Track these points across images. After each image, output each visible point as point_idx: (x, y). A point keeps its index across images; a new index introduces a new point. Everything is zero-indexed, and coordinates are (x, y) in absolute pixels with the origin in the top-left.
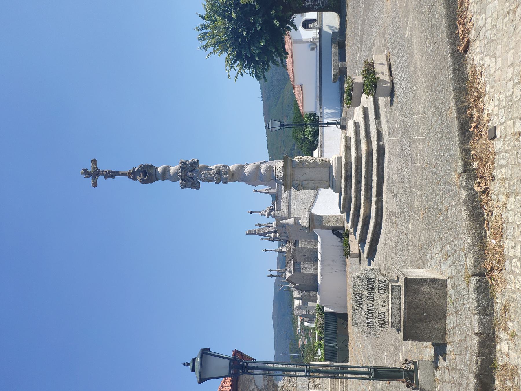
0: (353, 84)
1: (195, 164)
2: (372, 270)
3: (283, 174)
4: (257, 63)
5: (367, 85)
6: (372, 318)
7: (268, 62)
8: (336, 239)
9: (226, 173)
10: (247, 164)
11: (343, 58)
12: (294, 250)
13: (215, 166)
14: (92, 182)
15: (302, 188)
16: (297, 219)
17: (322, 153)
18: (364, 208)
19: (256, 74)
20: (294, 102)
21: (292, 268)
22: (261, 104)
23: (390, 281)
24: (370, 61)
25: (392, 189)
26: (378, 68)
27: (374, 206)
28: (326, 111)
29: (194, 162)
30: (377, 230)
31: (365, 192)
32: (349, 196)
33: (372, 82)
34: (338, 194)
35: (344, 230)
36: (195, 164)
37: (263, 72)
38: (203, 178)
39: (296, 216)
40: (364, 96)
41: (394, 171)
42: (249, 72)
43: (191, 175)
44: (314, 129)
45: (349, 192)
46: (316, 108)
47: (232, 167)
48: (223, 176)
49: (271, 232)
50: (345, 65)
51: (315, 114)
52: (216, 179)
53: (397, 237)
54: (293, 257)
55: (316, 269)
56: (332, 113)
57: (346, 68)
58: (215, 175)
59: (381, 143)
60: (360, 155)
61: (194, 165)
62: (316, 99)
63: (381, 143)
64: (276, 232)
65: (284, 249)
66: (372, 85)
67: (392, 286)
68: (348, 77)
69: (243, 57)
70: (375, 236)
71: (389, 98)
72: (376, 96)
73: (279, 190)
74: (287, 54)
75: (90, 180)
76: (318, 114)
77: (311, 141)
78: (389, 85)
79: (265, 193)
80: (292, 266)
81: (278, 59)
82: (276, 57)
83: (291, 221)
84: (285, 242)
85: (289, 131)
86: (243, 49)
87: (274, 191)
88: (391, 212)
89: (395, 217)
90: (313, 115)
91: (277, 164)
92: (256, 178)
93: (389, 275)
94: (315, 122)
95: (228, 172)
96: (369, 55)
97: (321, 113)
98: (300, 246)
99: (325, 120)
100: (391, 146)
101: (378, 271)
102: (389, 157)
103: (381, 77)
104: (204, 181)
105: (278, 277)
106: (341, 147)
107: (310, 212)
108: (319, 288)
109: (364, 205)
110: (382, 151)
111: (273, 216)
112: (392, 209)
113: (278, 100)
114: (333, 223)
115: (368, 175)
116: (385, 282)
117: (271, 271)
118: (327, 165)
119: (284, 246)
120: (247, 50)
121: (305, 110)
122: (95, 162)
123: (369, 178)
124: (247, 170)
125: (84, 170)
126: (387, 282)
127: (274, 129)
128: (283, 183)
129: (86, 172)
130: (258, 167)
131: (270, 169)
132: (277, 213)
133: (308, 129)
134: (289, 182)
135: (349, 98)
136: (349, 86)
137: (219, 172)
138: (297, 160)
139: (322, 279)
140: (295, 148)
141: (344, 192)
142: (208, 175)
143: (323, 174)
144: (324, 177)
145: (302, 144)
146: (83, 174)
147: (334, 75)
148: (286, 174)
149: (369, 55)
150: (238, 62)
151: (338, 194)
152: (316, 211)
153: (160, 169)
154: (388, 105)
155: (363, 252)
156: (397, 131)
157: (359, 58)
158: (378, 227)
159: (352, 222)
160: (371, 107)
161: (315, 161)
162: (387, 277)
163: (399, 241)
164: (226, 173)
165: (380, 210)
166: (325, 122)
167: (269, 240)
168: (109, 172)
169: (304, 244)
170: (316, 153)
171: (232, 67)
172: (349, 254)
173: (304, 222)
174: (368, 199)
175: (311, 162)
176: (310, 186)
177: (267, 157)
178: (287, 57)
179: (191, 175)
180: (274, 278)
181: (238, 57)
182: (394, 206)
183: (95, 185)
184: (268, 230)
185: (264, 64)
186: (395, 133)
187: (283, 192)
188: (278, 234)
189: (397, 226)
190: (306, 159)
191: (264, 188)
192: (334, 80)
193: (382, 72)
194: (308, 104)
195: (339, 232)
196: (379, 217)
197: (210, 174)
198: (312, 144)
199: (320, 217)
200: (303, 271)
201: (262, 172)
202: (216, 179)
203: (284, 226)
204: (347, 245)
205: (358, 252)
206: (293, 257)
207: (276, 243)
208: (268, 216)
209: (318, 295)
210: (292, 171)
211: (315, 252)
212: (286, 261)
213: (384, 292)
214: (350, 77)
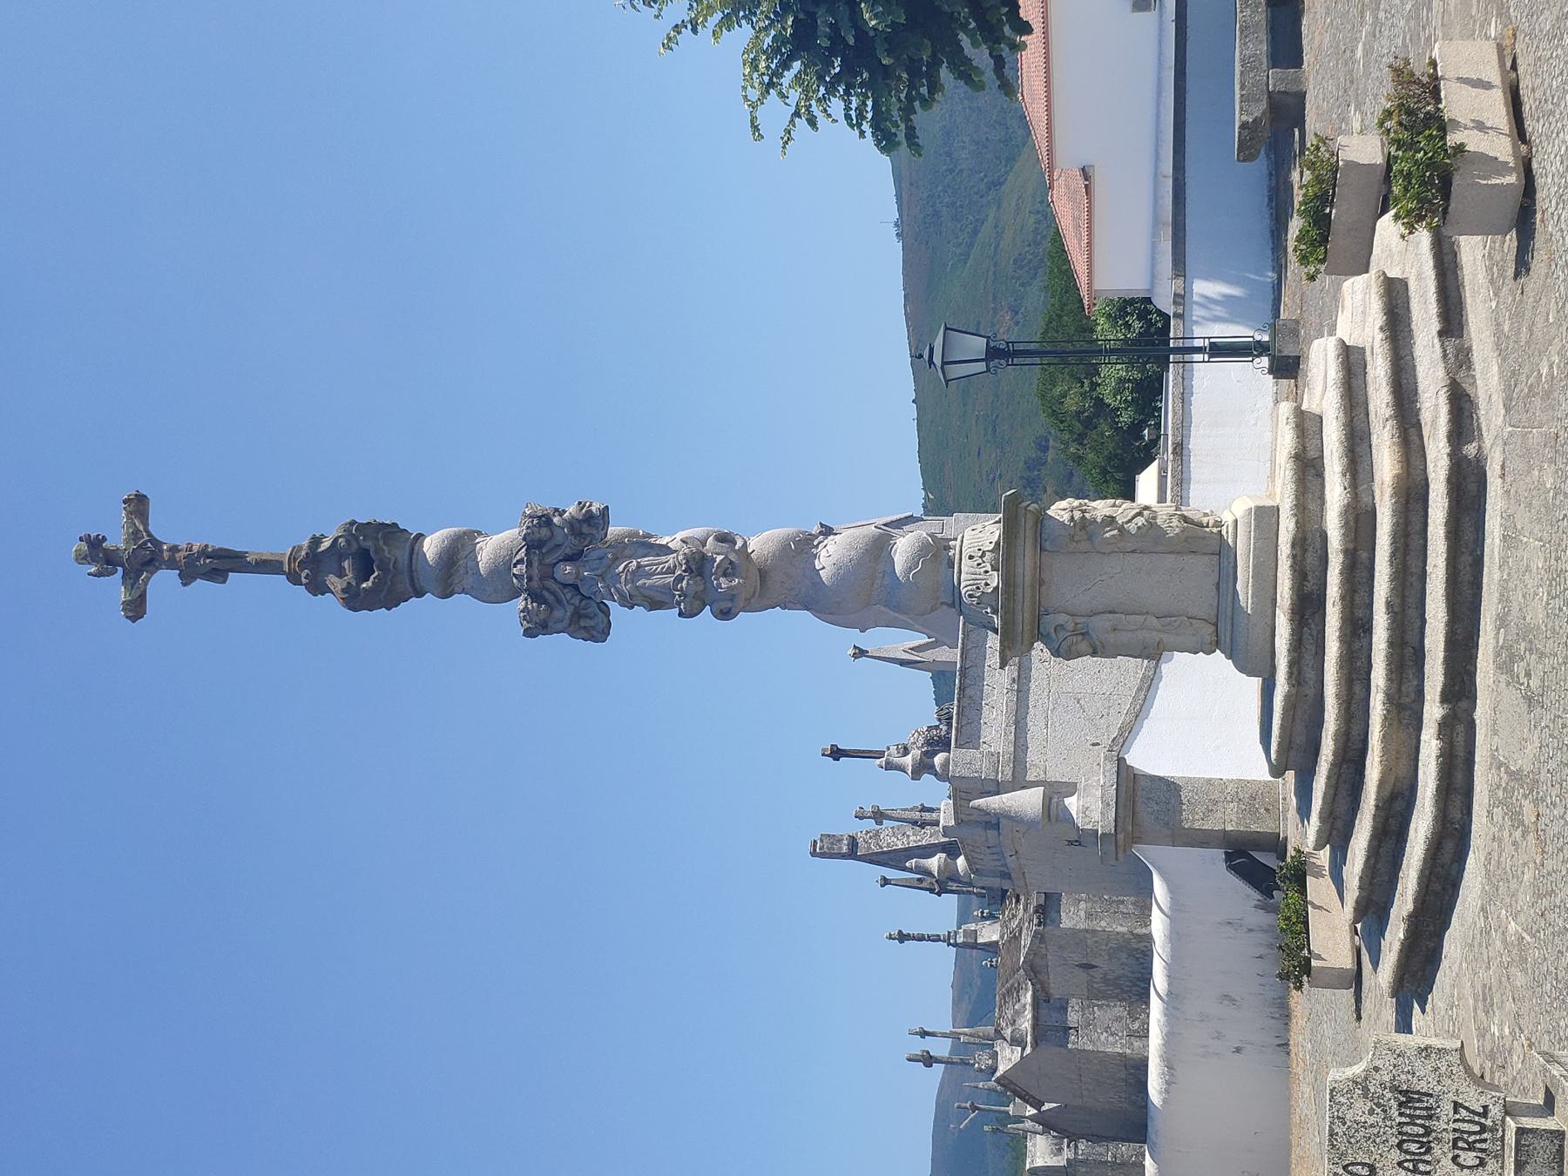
0: (1335, 169)
1: (592, 522)
2: (1425, 1051)
3: (994, 580)
4: (880, 81)
5: (1408, 177)
6: (1426, 1158)
7: (935, 64)
8: (1239, 896)
9: (729, 570)
10: (827, 531)
11: (1286, 46)
12: (1039, 938)
13: (680, 535)
14: (122, 594)
15: (1084, 646)
16: (1056, 792)
17: (1177, 484)
18: (1385, 751)
19: (875, 125)
20: (1047, 244)
21: (1026, 1024)
22: (892, 253)
23: (1508, 1110)
24: (1420, 69)
25: (1519, 668)
26: (1457, 103)
27: (1430, 746)
28: (1202, 288)
29: (589, 518)
30: (1446, 857)
31: (1389, 679)
32: (1311, 692)
33: (1431, 164)
34: (1256, 682)
35: (1282, 855)
36: (592, 522)
37: (908, 111)
38: (626, 589)
39: (1054, 776)
40: (1387, 228)
41: (1530, 583)
42: (848, 108)
43: (569, 576)
44: (1143, 370)
45: (1310, 675)
46: (1153, 276)
47: (760, 543)
48: (716, 583)
49: (927, 851)
50: (1298, 81)
51: (1148, 300)
52: (684, 594)
53: (1541, 896)
54: (1034, 970)
55: (1144, 1034)
56: (1227, 301)
57: (1301, 96)
58: (680, 579)
59: (1470, 450)
60: (1365, 499)
61: (585, 529)
62: (1155, 234)
63: (1470, 450)
64: (951, 850)
65: (990, 933)
66: (1427, 175)
67: (1521, 1132)
68: (1310, 140)
69: (824, 42)
70: (1437, 887)
71: (1511, 240)
72: (1446, 231)
73: (972, 654)
74: (1026, 28)
75: (115, 588)
76: (1164, 303)
77: (1125, 418)
78: (1511, 179)
79: (903, 663)
80: (1028, 1014)
81: (980, 56)
82: (975, 44)
83: (1027, 801)
84: (995, 900)
85: (1024, 379)
86: (821, 11)
87: (950, 655)
88: (1516, 776)
89: (1536, 802)
90: (1137, 307)
91: (968, 533)
92: (865, 595)
93: (1500, 1079)
94: (1151, 339)
95: (738, 563)
96: (1415, 38)
97: (1179, 299)
98: (1067, 922)
99: (1198, 331)
100: (1515, 464)
101: (1455, 1058)
102: (1508, 518)
103: (1475, 142)
104: (628, 602)
105: (958, 1063)
106: (1273, 462)
107: (1121, 761)
108: (1156, 1126)
109: (1385, 739)
110: (1472, 487)
111: (943, 776)
112: (1522, 762)
113: (975, 232)
114: (1229, 820)
115: (1403, 597)
116: (1485, 1114)
117: (924, 1034)
118: (1205, 545)
119: (991, 917)
120: (843, 9)
121: (1097, 286)
122: (138, 505)
123: (1412, 613)
124: (829, 556)
125: (87, 539)
126: (1495, 1111)
127: (957, 371)
128: (997, 621)
129: (97, 553)
130: (879, 547)
131: (938, 554)
132: (958, 760)
133: (1112, 373)
134: (1024, 615)
135: (1314, 233)
136: (1318, 180)
137: (698, 564)
138: (1066, 517)
139: (1169, 1084)
140: (1051, 455)
141: (1290, 674)
142: (650, 575)
143: (1190, 585)
144: (1189, 592)
146: (81, 558)
147: (1244, 126)
148: (1009, 582)
149: (1415, 38)
150: (797, 65)
151: (1256, 682)
152: (1146, 757)
153: (431, 547)
154: (1502, 271)
155: (1375, 963)
156: (1548, 394)
157: (1366, 53)
158: (1449, 846)
159: (1321, 818)
160: (1419, 277)
161: (1152, 524)
162: (1497, 1088)
163: (1551, 916)
164: (729, 570)
165: (1459, 762)
166: (1198, 343)
167: (917, 885)
168: (204, 552)
169: (1089, 916)
170: (1147, 483)
171: (771, 84)
172: (1306, 968)
173: (1090, 807)
174: (1406, 711)
175: (1132, 527)
177: (913, 497)
178: (1023, 46)
179: (569, 576)
180: (939, 1069)
181: (800, 43)
182: (1531, 750)
183: (136, 609)
184: (915, 838)
185: (915, 73)
186: (1537, 401)
187: (993, 659)
188: (961, 862)
189: (1542, 843)
190: (1108, 511)
191: (902, 641)
192: (1247, 151)
193: (1476, 119)
194: (1117, 255)
195: (1259, 864)
196: (1457, 800)
197: (659, 572)
198: (1127, 440)
199: (1168, 789)
200: (1076, 1042)
201: (899, 568)
202: (684, 594)
203: (994, 822)
204: (1299, 925)
205: (1347, 962)
206: (1034, 970)
207: (950, 903)
208: (917, 773)
209: (1148, 1161)
210: (1039, 568)
211: (1141, 952)
212: (1000, 990)
213: (1482, 1163)
214: (1323, 140)
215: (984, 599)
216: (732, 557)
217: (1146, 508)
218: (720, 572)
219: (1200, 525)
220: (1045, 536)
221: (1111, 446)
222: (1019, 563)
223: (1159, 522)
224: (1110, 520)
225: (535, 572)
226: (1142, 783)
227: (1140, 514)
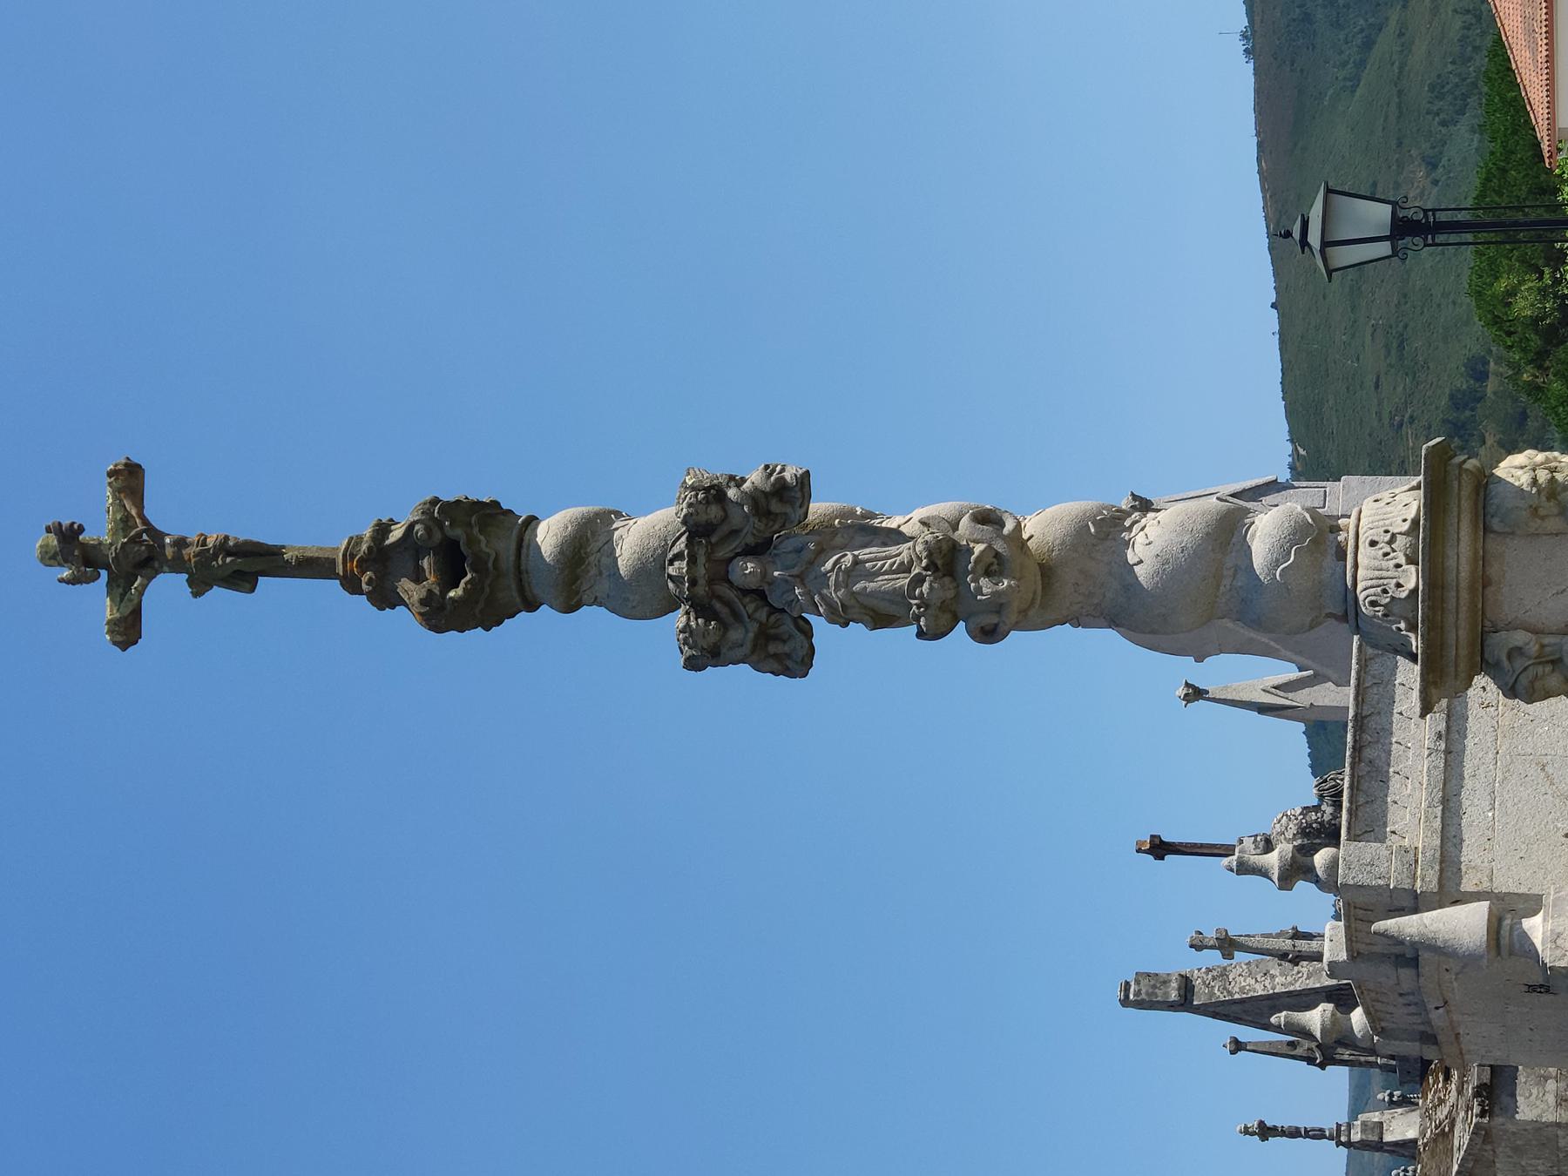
3: (1411, 578)
9: (994, 566)
43: (752, 576)
52: (924, 603)
58: (918, 581)
61: (775, 506)
129: (71, 550)
134: (1459, 634)
140: (1491, 386)
145: (1539, 360)
146: (49, 558)
164: (994, 566)
179: (752, 576)
183: (127, 630)
210: (1482, 560)
215: (1396, 609)
216: (999, 546)
218: (980, 570)
220: (1491, 510)
222: (1451, 553)
225: (701, 571)
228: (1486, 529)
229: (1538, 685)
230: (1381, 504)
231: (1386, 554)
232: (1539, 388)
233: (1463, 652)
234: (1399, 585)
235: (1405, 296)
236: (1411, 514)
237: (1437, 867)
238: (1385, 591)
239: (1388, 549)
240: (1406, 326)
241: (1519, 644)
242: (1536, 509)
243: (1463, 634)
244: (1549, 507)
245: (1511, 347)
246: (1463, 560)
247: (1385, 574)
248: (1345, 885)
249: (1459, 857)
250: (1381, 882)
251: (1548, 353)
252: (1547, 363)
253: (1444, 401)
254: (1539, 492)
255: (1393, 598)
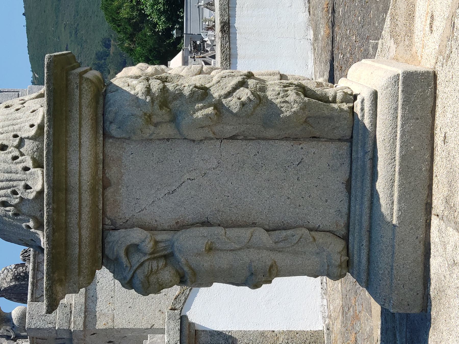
3: (38, 181)
77: (160, 27)
107: (183, 319)
134: (82, 232)
140: (112, 49)
145: (131, 37)
175: (233, 103)
176: (223, 261)
210: (102, 163)
215: (25, 209)
217: (250, 75)
219: (324, 99)
220: (110, 116)
221: (151, 42)
222: (73, 157)
223: (270, 94)
224: (202, 93)
226: (203, 338)
227: (242, 84)
228: (106, 135)
229: (153, 279)
230: (12, 110)
231: (15, 158)
232: (131, 50)
233: (86, 250)
234: (27, 187)
235: (77, 12)
236: (37, 120)
237: (83, 315)
238: (15, 193)
239: (16, 153)
240: (78, 25)
241: (135, 241)
242: (150, 116)
243: (85, 233)
244: (161, 115)
245: (119, 32)
246: (85, 164)
247: (14, 176)
248: (30, 329)
249: (95, 308)
250: (51, 326)
251: (135, 34)
252: (135, 39)
253: (93, 56)
254: (152, 101)
255: (22, 199)
